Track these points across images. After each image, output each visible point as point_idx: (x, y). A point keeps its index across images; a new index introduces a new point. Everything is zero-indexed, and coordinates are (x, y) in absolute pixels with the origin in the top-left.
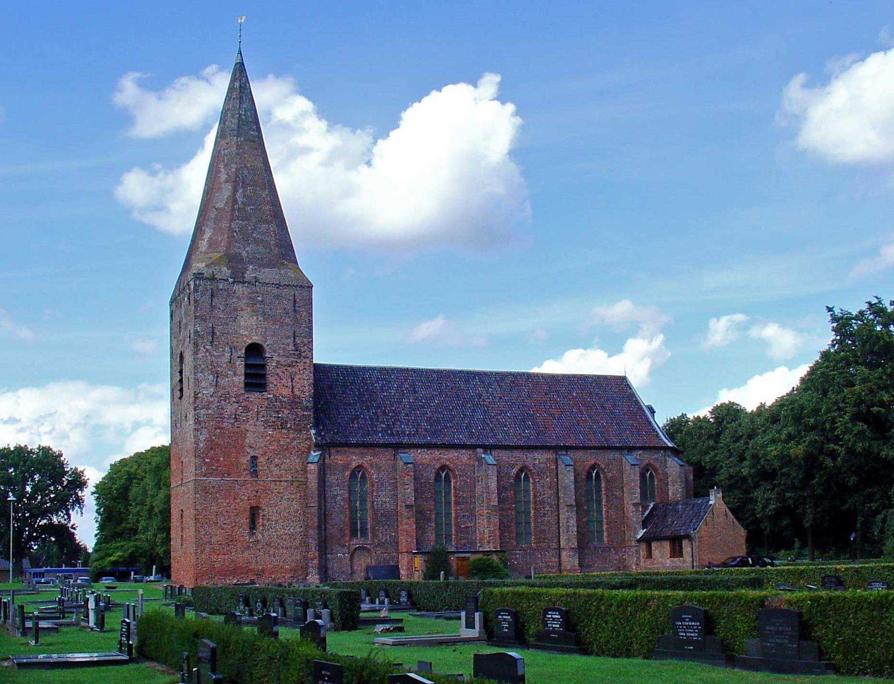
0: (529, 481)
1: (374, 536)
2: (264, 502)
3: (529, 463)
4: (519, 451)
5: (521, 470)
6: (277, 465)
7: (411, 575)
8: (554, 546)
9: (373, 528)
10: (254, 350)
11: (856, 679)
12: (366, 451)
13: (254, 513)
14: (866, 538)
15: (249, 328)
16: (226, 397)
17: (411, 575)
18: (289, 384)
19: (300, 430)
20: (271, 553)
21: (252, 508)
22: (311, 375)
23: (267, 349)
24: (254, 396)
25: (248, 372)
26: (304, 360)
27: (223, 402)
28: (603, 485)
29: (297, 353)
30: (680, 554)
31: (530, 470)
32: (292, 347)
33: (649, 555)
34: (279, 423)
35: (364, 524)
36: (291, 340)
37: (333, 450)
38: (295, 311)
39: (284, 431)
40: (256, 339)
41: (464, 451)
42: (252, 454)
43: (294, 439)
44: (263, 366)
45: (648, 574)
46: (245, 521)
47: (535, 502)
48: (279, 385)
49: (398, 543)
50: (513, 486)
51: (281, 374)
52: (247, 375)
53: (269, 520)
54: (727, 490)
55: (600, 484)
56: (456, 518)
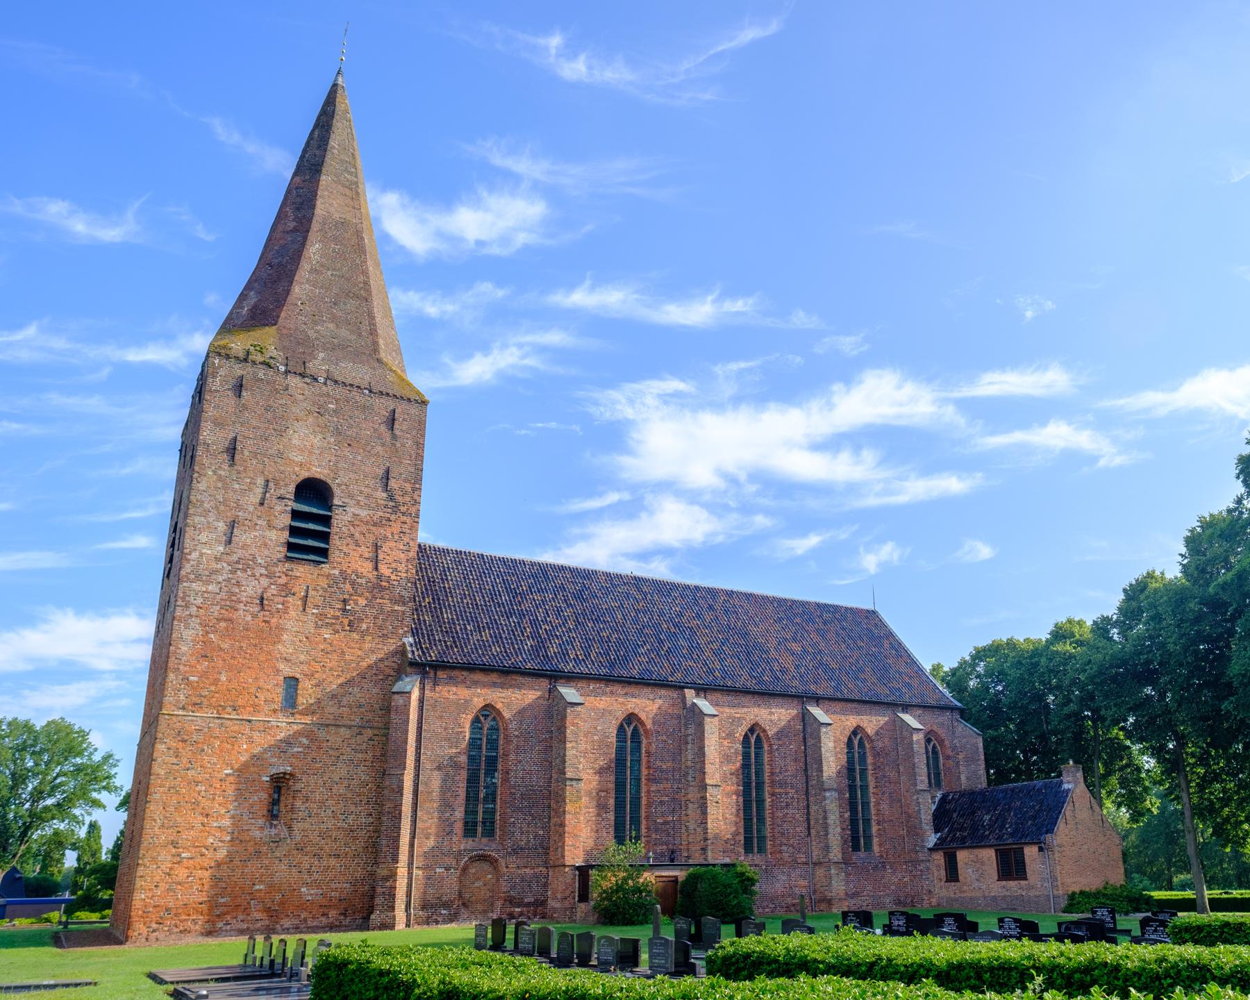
5: (752, 730)
16: (246, 565)
24: (304, 572)
33: (952, 874)
39: (355, 635)
42: (287, 670)
47: (772, 782)
56: (649, 805)
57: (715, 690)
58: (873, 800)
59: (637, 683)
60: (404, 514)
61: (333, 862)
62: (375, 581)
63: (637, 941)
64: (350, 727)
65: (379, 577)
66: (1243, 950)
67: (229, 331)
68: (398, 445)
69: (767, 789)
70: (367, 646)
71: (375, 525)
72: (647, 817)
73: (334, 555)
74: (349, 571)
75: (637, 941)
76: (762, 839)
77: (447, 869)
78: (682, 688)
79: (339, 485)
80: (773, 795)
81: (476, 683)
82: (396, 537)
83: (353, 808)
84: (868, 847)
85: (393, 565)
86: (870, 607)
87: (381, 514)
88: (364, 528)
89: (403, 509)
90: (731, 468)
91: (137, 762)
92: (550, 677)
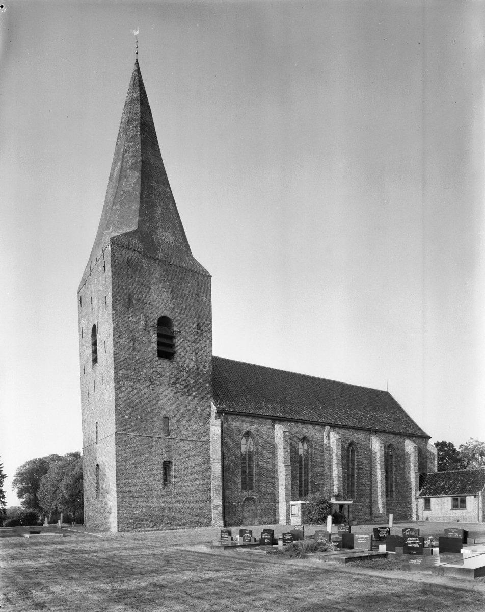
0: (354, 453)
1: (258, 489)
2: (174, 458)
3: (355, 439)
5: (350, 445)
6: (184, 427)
7: (288, 520)
8: (368, 500)
9: (258, 482)
10: (164, 322)
13: (167, 465)
15: (159, 301)
17: (288, 520)
20: (181, 501)
21: (165, 462)
23: (175, 323)
24: (165, 363)
26: (205, 339)
27: (139, 365)
29: (199, 332)
30: (463, 506)
31: (356, 445)
32: (195, 326)
33: (428, 506)
35: (251, 479)
36: (195, 320)
39: (190, 398)
40: (166, 313)
42: (165, 413)
43: (198, 405)
46: (159, 472)
49: (275, 495)
50: (349, 451)
52: (159, 344)
53: (179, 473)
54: (333, 516)
56: (312, 477)
57: (338, 427)
59: (307, 423)
61: (192, 500)
62: (196, 371)
64: (192, 441)
65: (198, 369)
69: (355, 471)
70: (196, 403)
71: (194, 342)
72: (311, 482)
74: (185, 366)
76: (251, 483)
78: (324, 426)
79: (176, 321)
80: (358, 473)
81: (243, 421)
82: (203, 349)
83: (197, 477)
87: (196, 337)
89: (205, 334)
90: (5, 479)
91: (412, 421)
92: (272, 419)
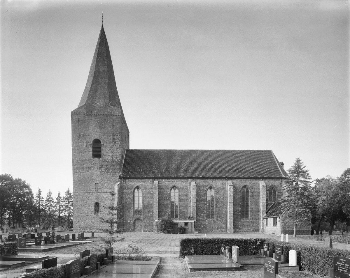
4: (209, 180)
8: (224, 220)
11: (203, 256)
12: (140, 180)
14: (204, 227)
18: (111, 152)
19: (115, 173)
22: (120, 151)
23: (101, 141)
24: (96, 160)
25: (95, 154)
28: (250, 194)
29: (114, 142)
32: (111, 140)
34: (106, 170)
37: (127, 180)
38: (113, 125)
39: (108, 173)
41: (183, 180)
44: (100, 148)
45: (215, 234)
48: (107, 153)
51: (107, 151)
55: (248, 194)
58: (228, 211)
60: (117, 144)
63: (273, 226)
65: (113, 159)
66: (348, 246)
67: (102, 265)
68: (114, 127)
70: (111, 175)
71: (111, 147)
73: (103, 157)
75: (273, 226)
77: (131, 221)
79: (102, 140)
84: (247, 217)
85: (116, 156)
86: (269, 149)
88: (108, 149)
89: (117, 143)
